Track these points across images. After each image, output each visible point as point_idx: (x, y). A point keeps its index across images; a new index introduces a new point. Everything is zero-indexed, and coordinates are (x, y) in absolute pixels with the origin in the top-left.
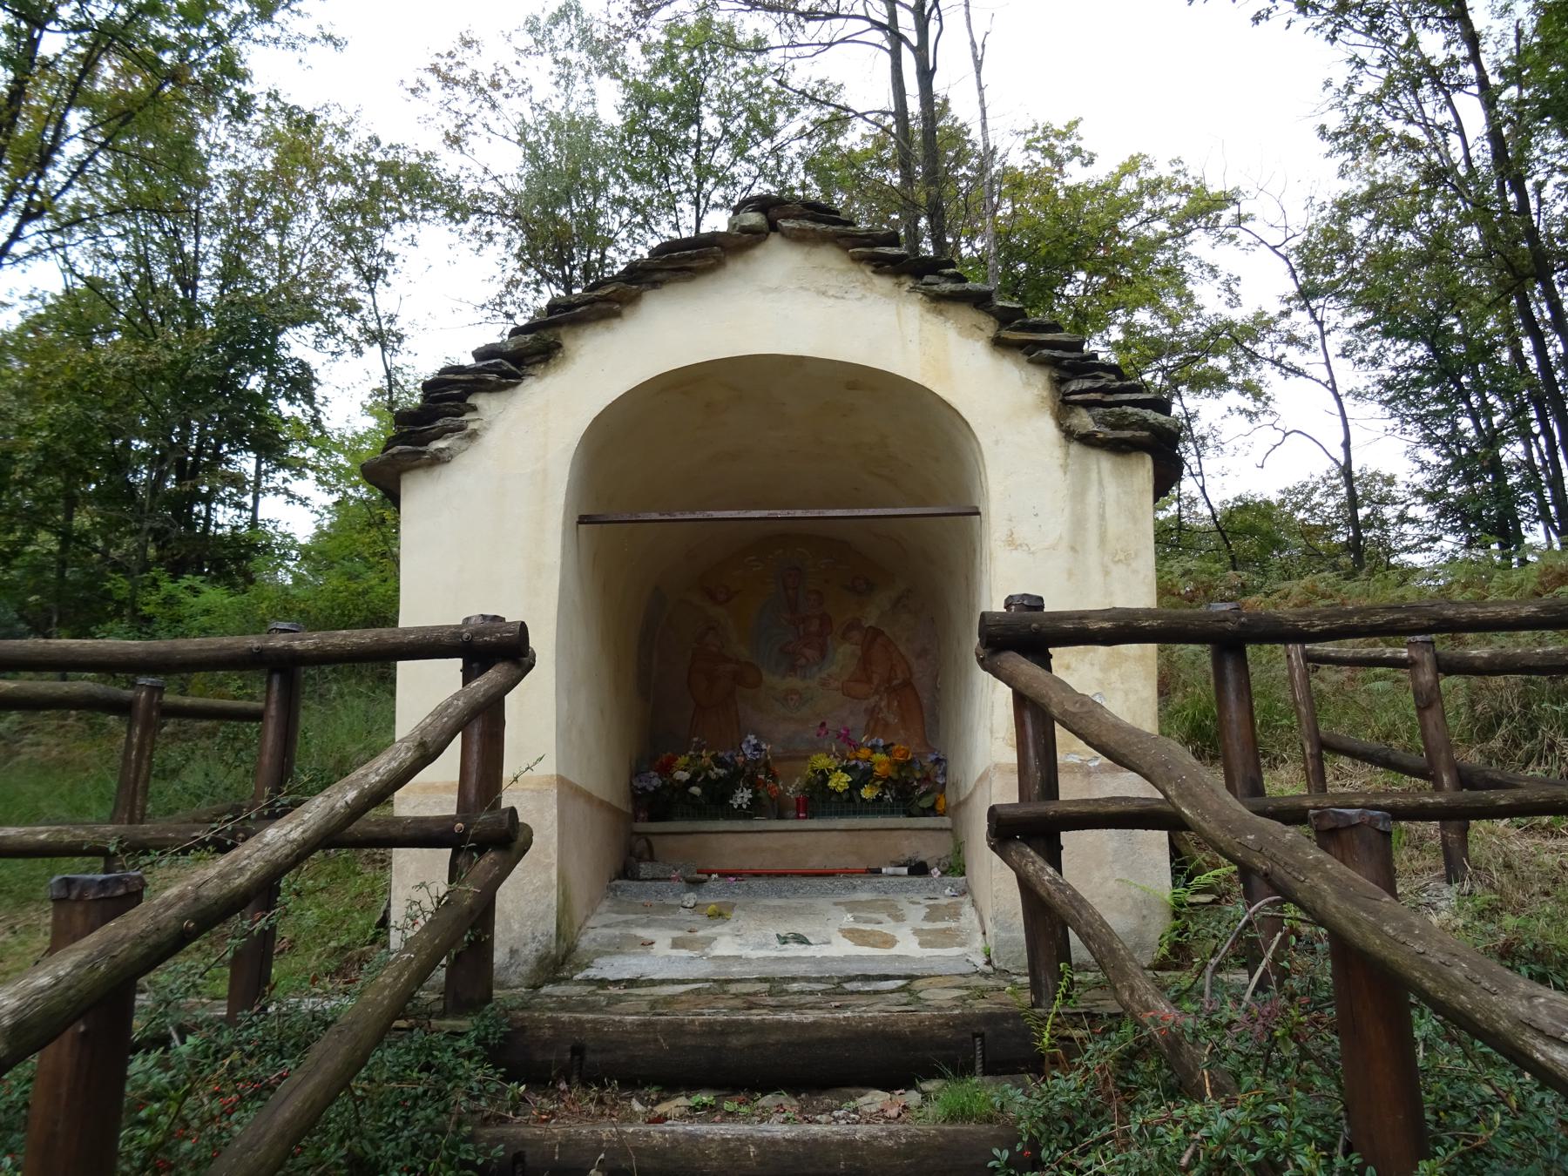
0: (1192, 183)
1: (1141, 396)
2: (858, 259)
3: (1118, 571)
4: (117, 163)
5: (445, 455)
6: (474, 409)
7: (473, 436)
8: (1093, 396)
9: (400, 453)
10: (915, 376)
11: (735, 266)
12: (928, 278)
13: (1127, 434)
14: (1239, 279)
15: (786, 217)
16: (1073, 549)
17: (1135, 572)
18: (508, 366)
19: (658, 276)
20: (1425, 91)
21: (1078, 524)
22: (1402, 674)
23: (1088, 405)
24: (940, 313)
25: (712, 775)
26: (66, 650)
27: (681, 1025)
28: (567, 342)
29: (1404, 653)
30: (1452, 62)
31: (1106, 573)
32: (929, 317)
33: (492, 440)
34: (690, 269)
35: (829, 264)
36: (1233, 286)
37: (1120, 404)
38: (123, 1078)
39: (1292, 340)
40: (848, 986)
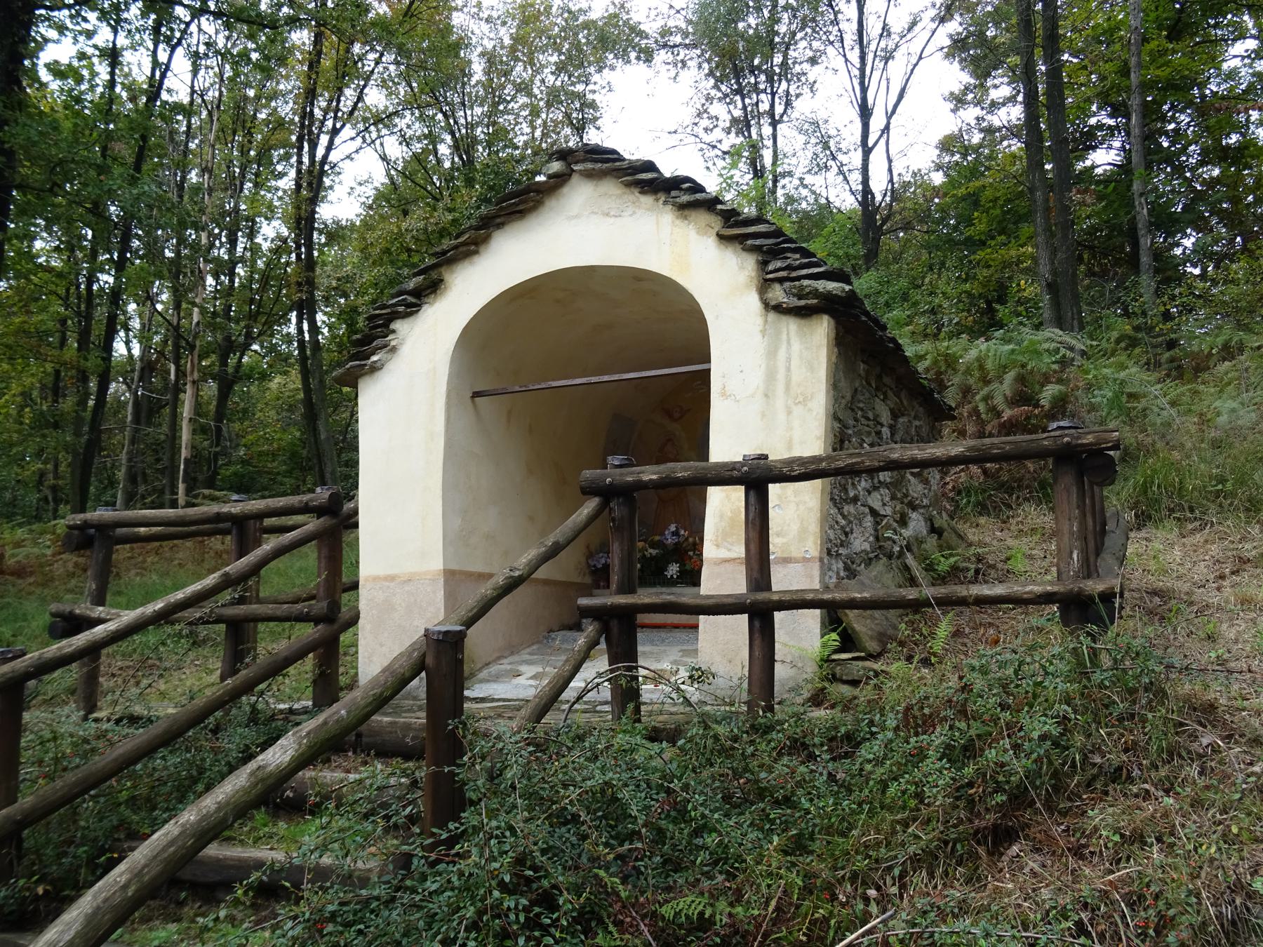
1: (816, 270)
3: (797, 411)
5: (378, 365)
6: (394, 331)
7: (394, 350)
11: (551, 203)
12: (673, 193)
15: (576, 163)
16: (766, 396)
17: (810, 410)
18: (411, 299)
19: (498, 220)
21: (771, 376)
23: (781, 281)
24: (686, 218)
26: (145, 517)
27: (410, 724)
31: (789, 413)
32: (678, 222)
34: (520, 212)
37: (799, 278)
38: (17, 729)
40: (598, 708)
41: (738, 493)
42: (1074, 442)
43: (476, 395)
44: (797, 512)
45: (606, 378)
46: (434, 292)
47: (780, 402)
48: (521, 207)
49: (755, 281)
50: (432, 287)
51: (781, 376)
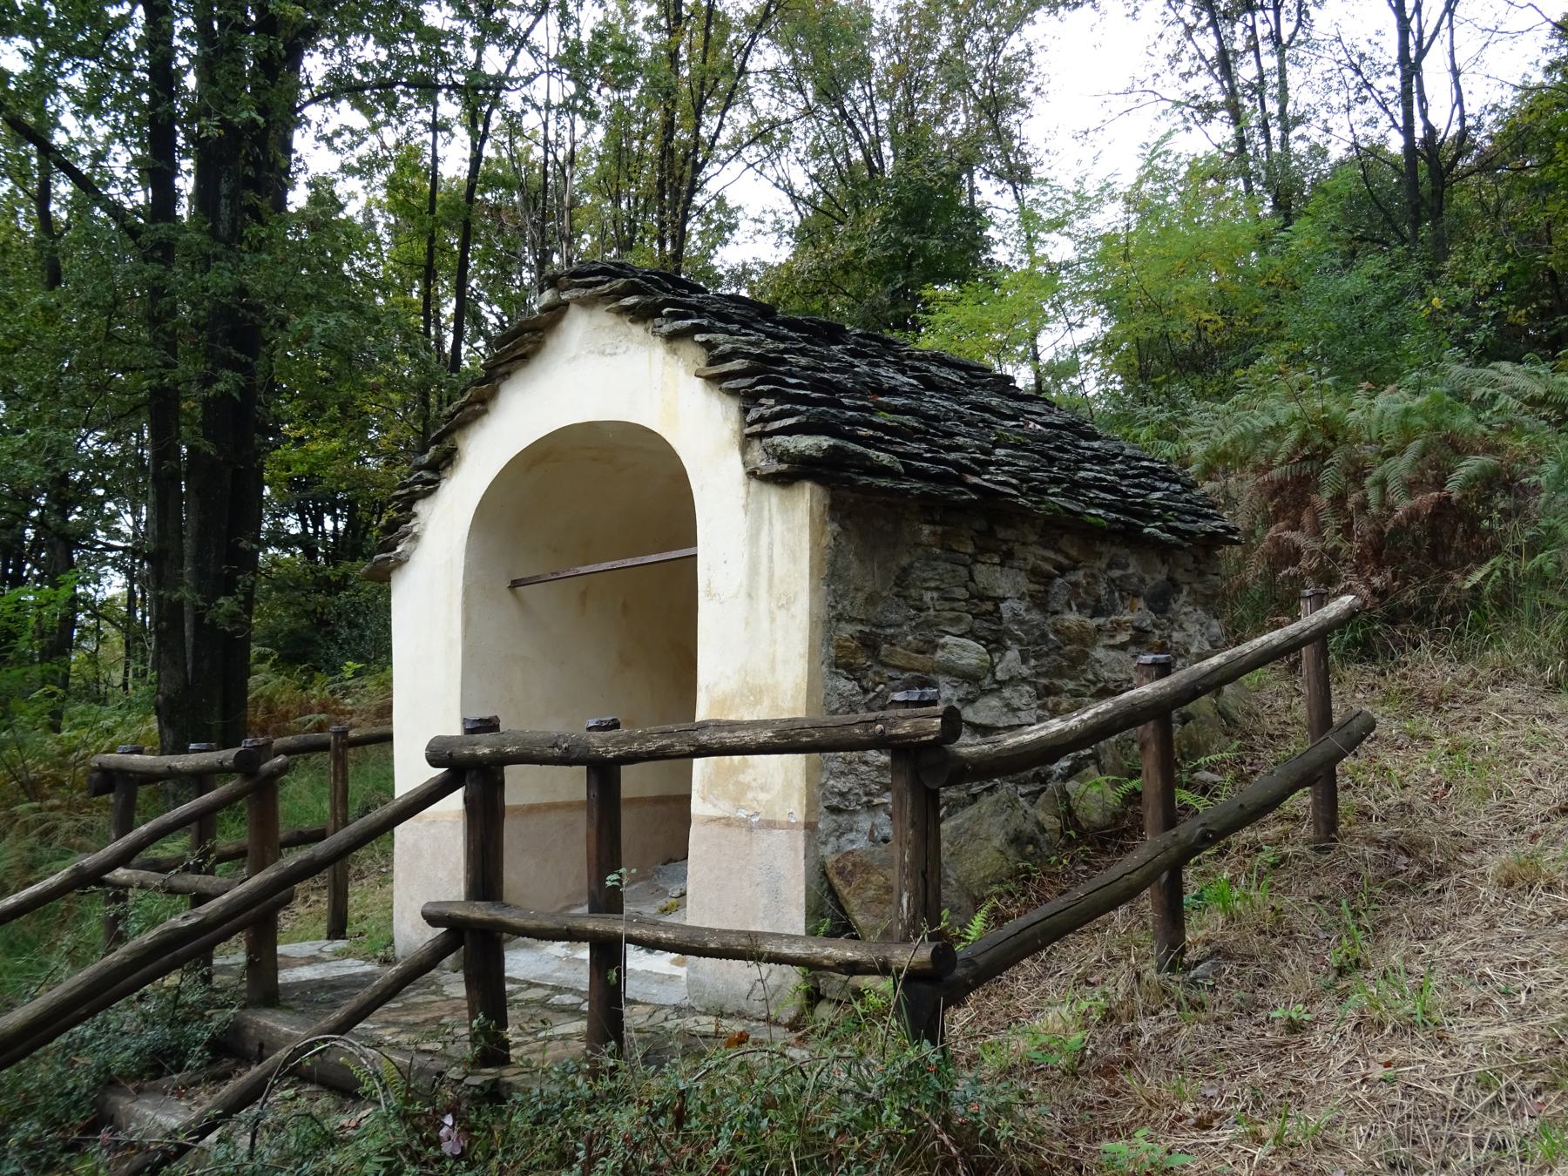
3: (781, 616)
6: (415, 515)
7: (416, 538)
11: (553, 342)
16: (750, 595)
17: (793, 616)
18: (427, 475)
19: (501, 370)
24: (674, 352)
25: (177, 23)
31: (773, 620)
32: (668, 358)
37: (771, 434)
42: (888, 732)
43: (515, 584)
47: (763, 603)
48: (519, 352)
50: (446, 460)
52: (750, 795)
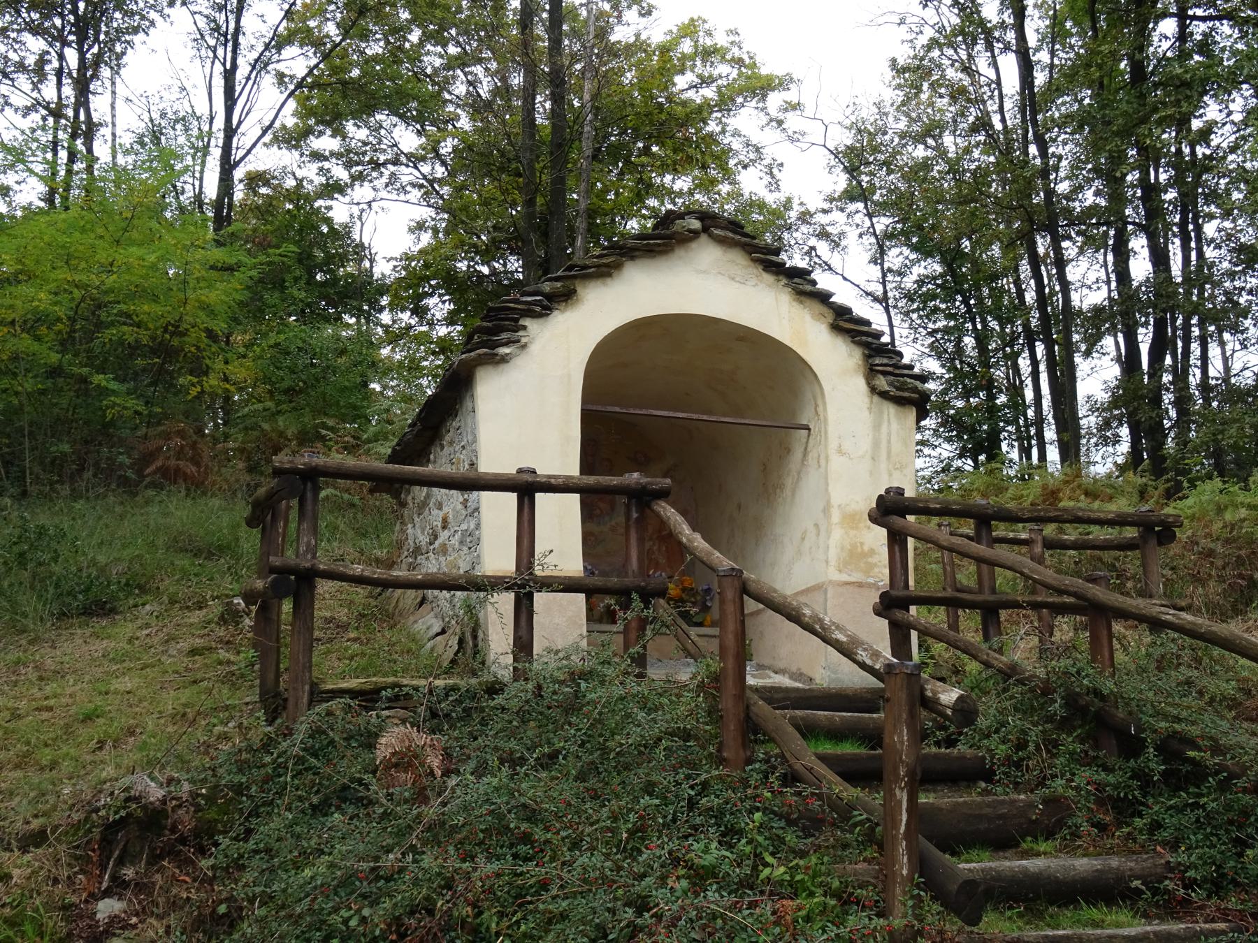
0: (745, 57)
2: (755, 261)
4: (41, 13)
6: (524, 328)
7: (524, 346)
8: (889, 369)
9: (485, 354)
10: (787, 341)
11: (680, 252)
12: (796, 280)
13: (906, 394)
14: (782, 165)
15: (716, 227)
18: (546, 303)
20: (980, 46)
21: (876, 444)
22: (1024, 549)
23: (884, 373)
24: (801, 302)
26: (414, 472)
28: (579, 289)
29: (1024, 536)
30: (1003, 26)
32: (795, 304)
33: (534, 348)
35: (736, 261)
36: (775, 171)
39: (823, 235)
41: (511, 498)
44: (560, 519)
45: (705, 417)
46: (566, 301)
47: (883, 466)
49: (862, 369)
51: (884, 445)
52: (876, 570)
